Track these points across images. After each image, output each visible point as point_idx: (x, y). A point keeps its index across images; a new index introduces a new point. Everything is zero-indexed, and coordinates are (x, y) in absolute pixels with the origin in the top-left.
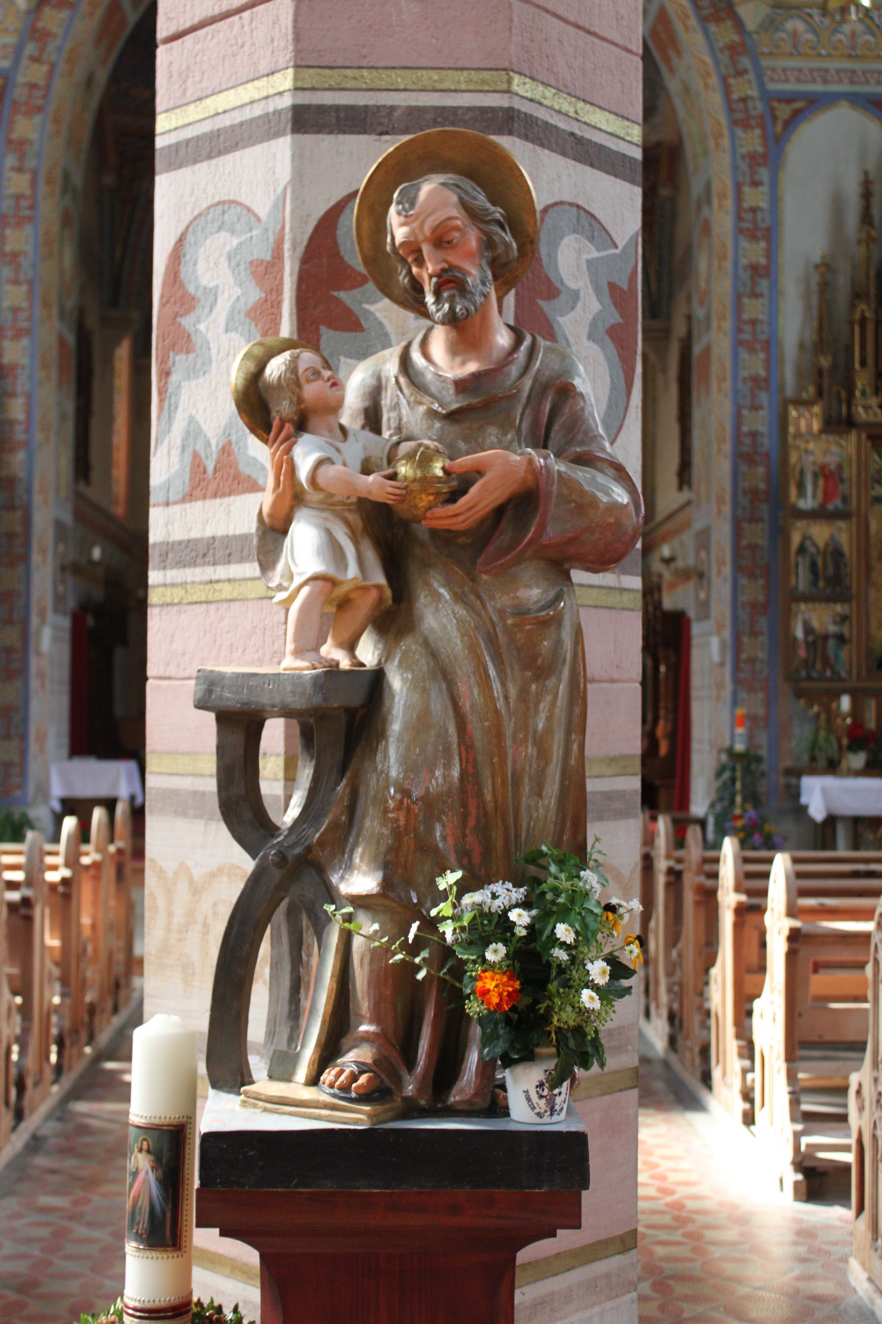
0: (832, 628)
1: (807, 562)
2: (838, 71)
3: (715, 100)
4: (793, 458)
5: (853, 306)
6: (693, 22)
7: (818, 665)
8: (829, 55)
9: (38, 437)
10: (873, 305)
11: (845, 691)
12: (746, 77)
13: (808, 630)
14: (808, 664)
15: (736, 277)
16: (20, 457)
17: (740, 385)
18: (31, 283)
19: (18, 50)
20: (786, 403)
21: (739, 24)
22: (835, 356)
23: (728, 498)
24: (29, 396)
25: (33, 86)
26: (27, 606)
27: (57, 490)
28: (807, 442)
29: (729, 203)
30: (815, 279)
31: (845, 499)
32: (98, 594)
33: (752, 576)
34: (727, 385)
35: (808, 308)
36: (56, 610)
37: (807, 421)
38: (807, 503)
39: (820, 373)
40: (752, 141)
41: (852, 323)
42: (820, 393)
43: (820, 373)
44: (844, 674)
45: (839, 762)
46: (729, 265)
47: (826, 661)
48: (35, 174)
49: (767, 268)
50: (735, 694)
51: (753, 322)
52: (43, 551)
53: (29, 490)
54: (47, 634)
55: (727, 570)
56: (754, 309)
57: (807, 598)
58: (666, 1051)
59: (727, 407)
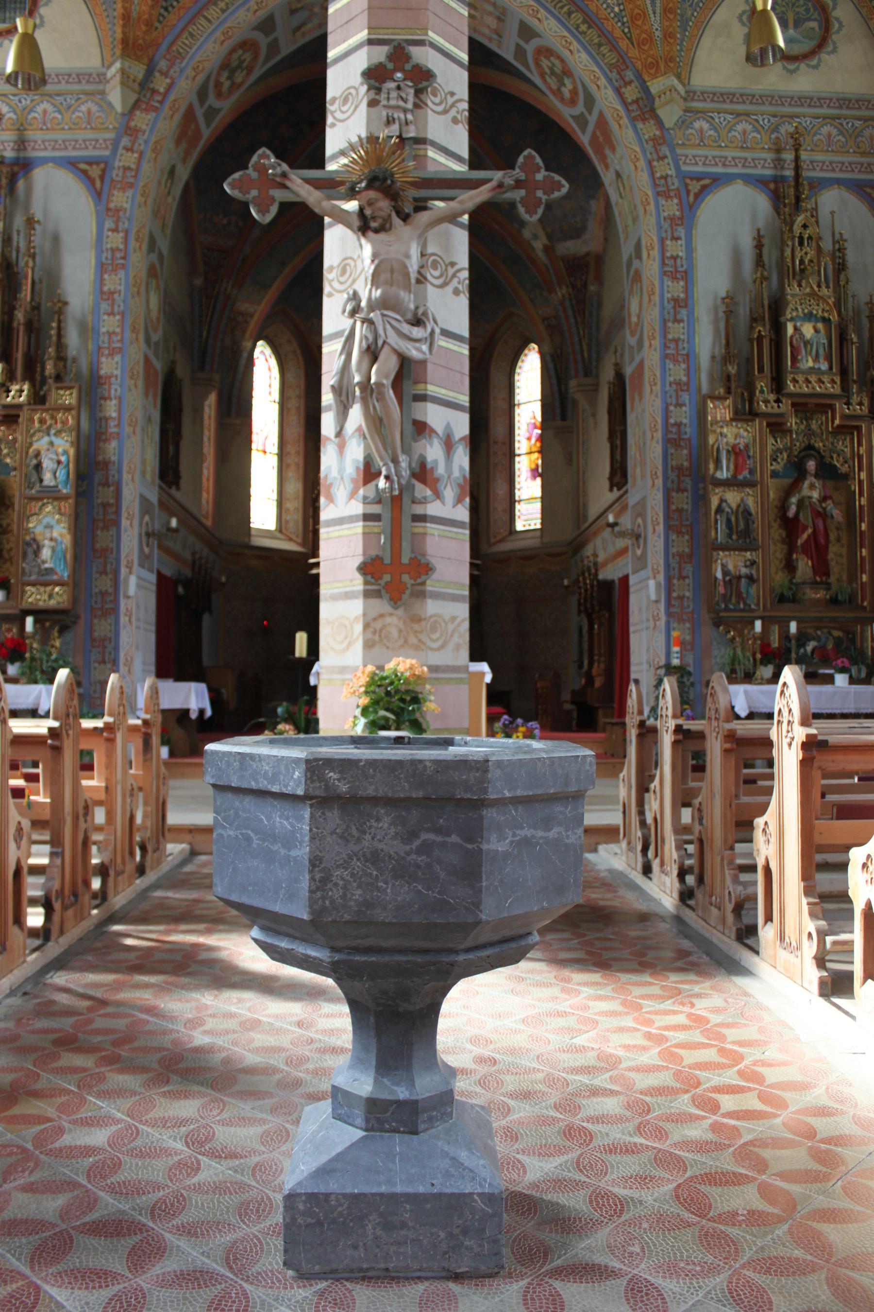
0: (744, 571)
1: (724, 520)
2: (734, 158)
3: (643, 178)
4: (711, 440)
5: (752, 328)
6: (625, 121)
7: (734, 600)
9: (128, 430)
10: (768, 327)
11: (758, 618)
12: (666, 161)
13: (725, 573)
14: (725, 598)
15: (663, 307)
16: (114, 444)
17: (668, 388)
18: (122, 314)
19: (116, 143)
20: (704, 399)
21: (660, 123)
22: (738, 365)
23: (660, 473)
24: (120, 399)
25: (126, 169)
26: (118, 560)
27: (143, 473)
28: (722, 427)
29: (656, 253)
30: (722, 308)
31: (752, 472)
32: (188, 572)
33: (679, 533)
34: (658, 388)
35: (717, 331)
36: (141, 565)
37: (720, 411)
38: (724, 474)
39: (728, 378)
40: (671, 207)
41: (751, 340)
42: (728, 391)
43: (728, 378)
44: (753, 607)
45: (754, 673)
46: (656, 298)
47: (739, 595)
48: (127, 232)
49: (686, 300)
50: (668, 623)
51: (676, 341)
52: (130, 518)
53: (120, 471)
54: (133, 581)
55: (660, 528)
56: (676, 331)
57: (724, 548)
58: (677, 908)
59: (658, 404)
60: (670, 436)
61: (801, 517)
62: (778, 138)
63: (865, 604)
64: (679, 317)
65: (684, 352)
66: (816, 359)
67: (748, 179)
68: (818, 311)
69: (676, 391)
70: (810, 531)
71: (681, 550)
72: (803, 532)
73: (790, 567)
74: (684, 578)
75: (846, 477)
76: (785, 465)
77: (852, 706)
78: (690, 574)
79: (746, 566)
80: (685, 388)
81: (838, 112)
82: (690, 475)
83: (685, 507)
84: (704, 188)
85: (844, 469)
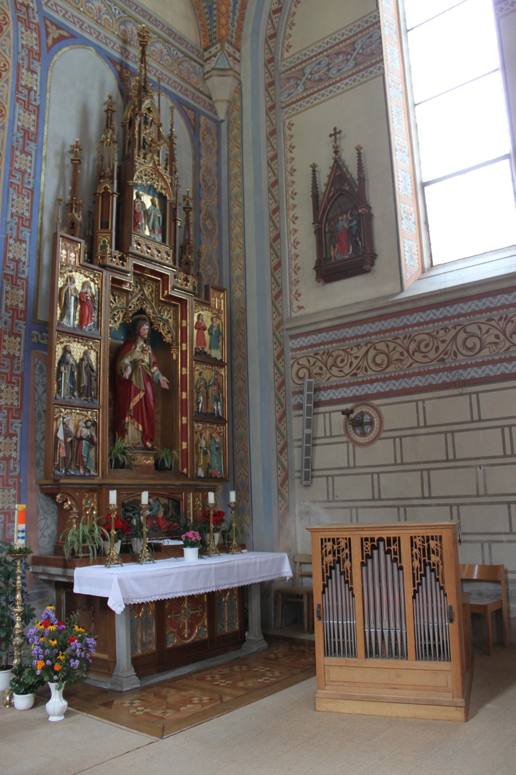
0: (86, 432)
4: (60, 283)
8: (83, 12)
13: (67, 434)
37: (69, 254)
56: (22, 162)
60: (7, 272)
61: (133, 379)
62: (125, 31)
63: (185, 470)
64: (27, 149)
65: (30, 187)
66: (152, 230)
67: (99, 51)
68: (159, 185)
69: (17, 224)
70: (142, 394)
71: (9, 402)
72: (135, 395)
73: (117, 429)
74: (12, 435)
75: (168, 346)
76: (121, 324)
77: (213, 584)
78: (18, 431)
79: (87, 427)
80: (27, 224)
81: (168, 37)
82: (24, 319)
83: (17, 354)
84: (61, 38)
85: (168, 339)
